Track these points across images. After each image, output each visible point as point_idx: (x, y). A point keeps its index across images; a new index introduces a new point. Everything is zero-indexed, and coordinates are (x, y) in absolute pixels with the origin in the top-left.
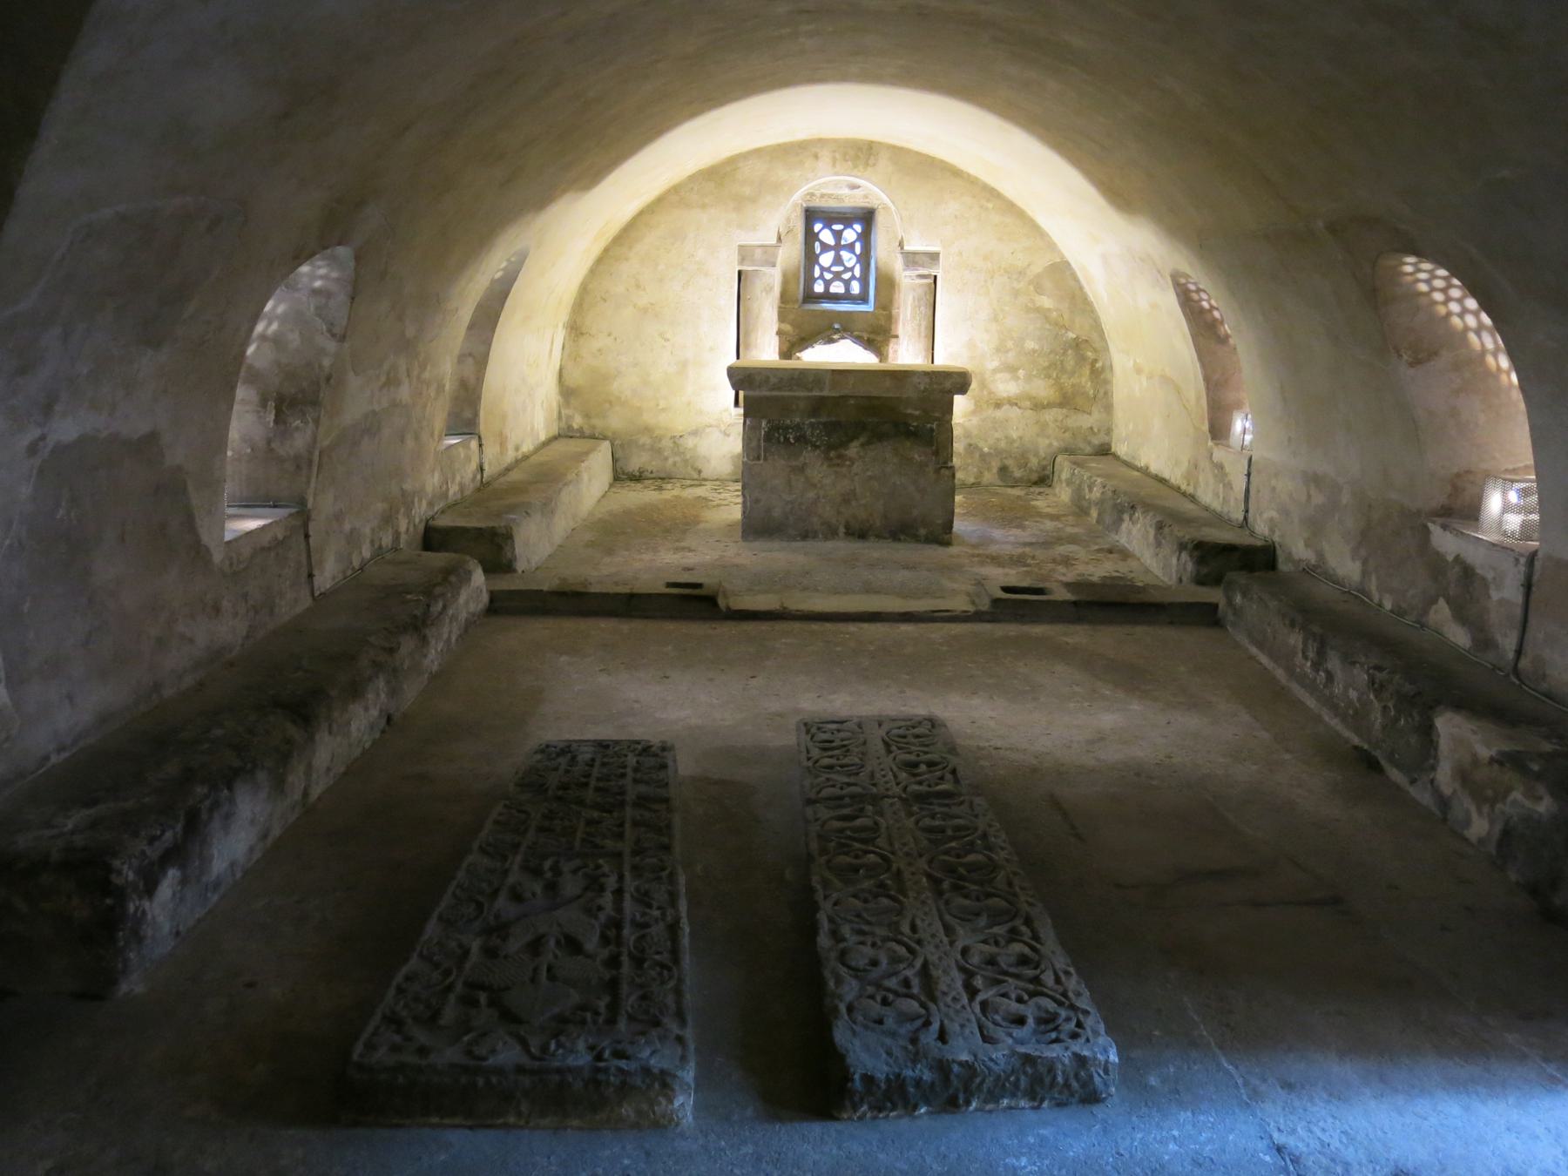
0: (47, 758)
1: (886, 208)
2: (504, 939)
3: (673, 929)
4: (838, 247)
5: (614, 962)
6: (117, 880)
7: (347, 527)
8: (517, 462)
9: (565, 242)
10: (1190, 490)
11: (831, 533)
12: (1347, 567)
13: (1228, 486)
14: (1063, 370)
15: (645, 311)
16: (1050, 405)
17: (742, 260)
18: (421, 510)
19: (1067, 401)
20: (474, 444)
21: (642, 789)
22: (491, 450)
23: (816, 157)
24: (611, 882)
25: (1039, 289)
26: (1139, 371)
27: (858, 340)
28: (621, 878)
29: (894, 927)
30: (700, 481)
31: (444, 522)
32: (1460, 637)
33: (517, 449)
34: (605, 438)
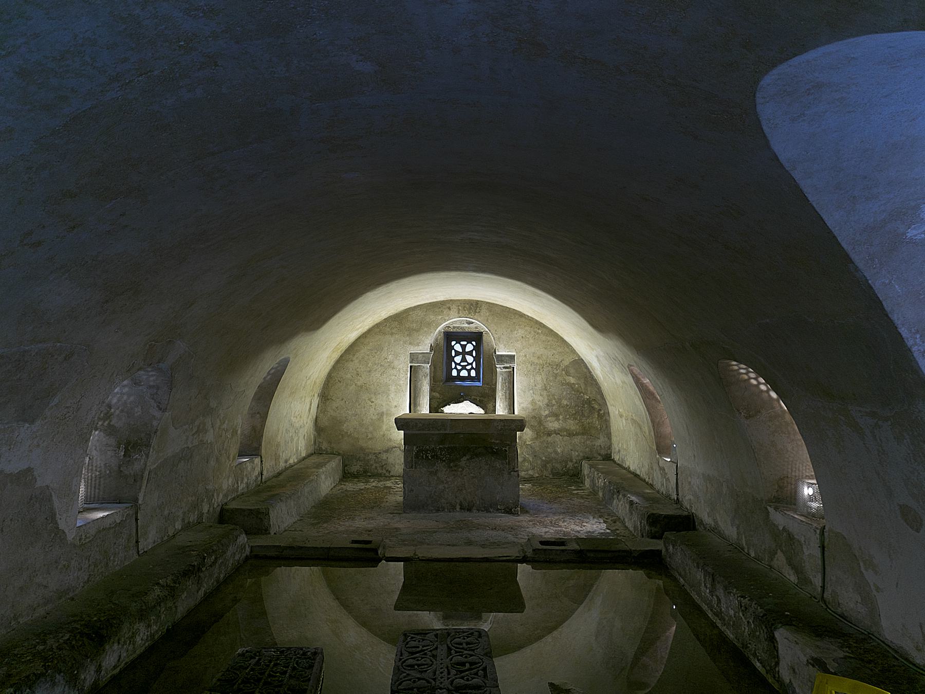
1: (487, 333)
4: (464, 353)
8: (286, 469)
9: (318, 354)
10: (650, 482)
11: (452, 508)
12: (731, 531)
13: (668, 480)
14: (583, 415)
15: (361, 387)
16: (577, 434)
18: (219, 499)
19: (585, 431)
23: (449, 308)
25: (568, 374)
26: (621, 416)
30: (389, 478)
31: (233, 505)
32: (793, 578)
33: (286, 461)
34: (339, 454)
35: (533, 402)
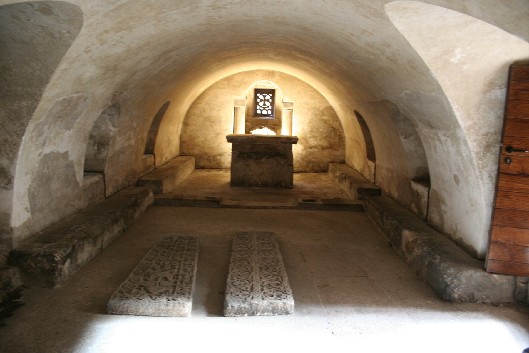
0: (38, 233)
2: (149, 277)
3: (191, 277)
5: (176, 282)
6: (56, 259)
7: (115, 179)
17: (235, 104)
19: (331, 147)
20: (153, 157)
21: (189, 247)
22: (158, 159)
23: (257, 74)
24: (177, 267)
27: (270, 128)
28: (180, 266)
29: (248, 278)
34: (193, 156)
35: (303, 130)
